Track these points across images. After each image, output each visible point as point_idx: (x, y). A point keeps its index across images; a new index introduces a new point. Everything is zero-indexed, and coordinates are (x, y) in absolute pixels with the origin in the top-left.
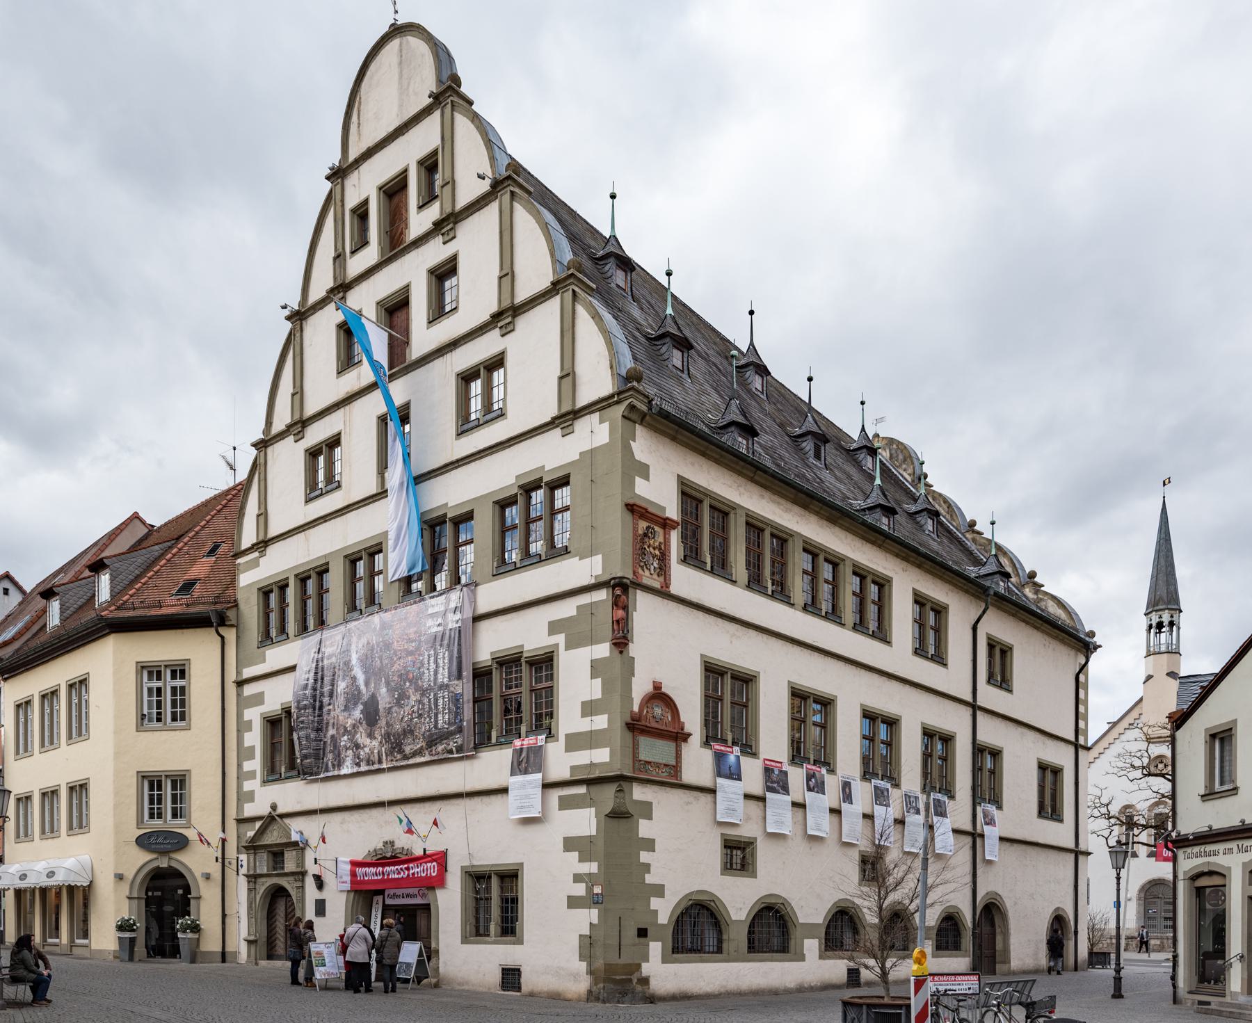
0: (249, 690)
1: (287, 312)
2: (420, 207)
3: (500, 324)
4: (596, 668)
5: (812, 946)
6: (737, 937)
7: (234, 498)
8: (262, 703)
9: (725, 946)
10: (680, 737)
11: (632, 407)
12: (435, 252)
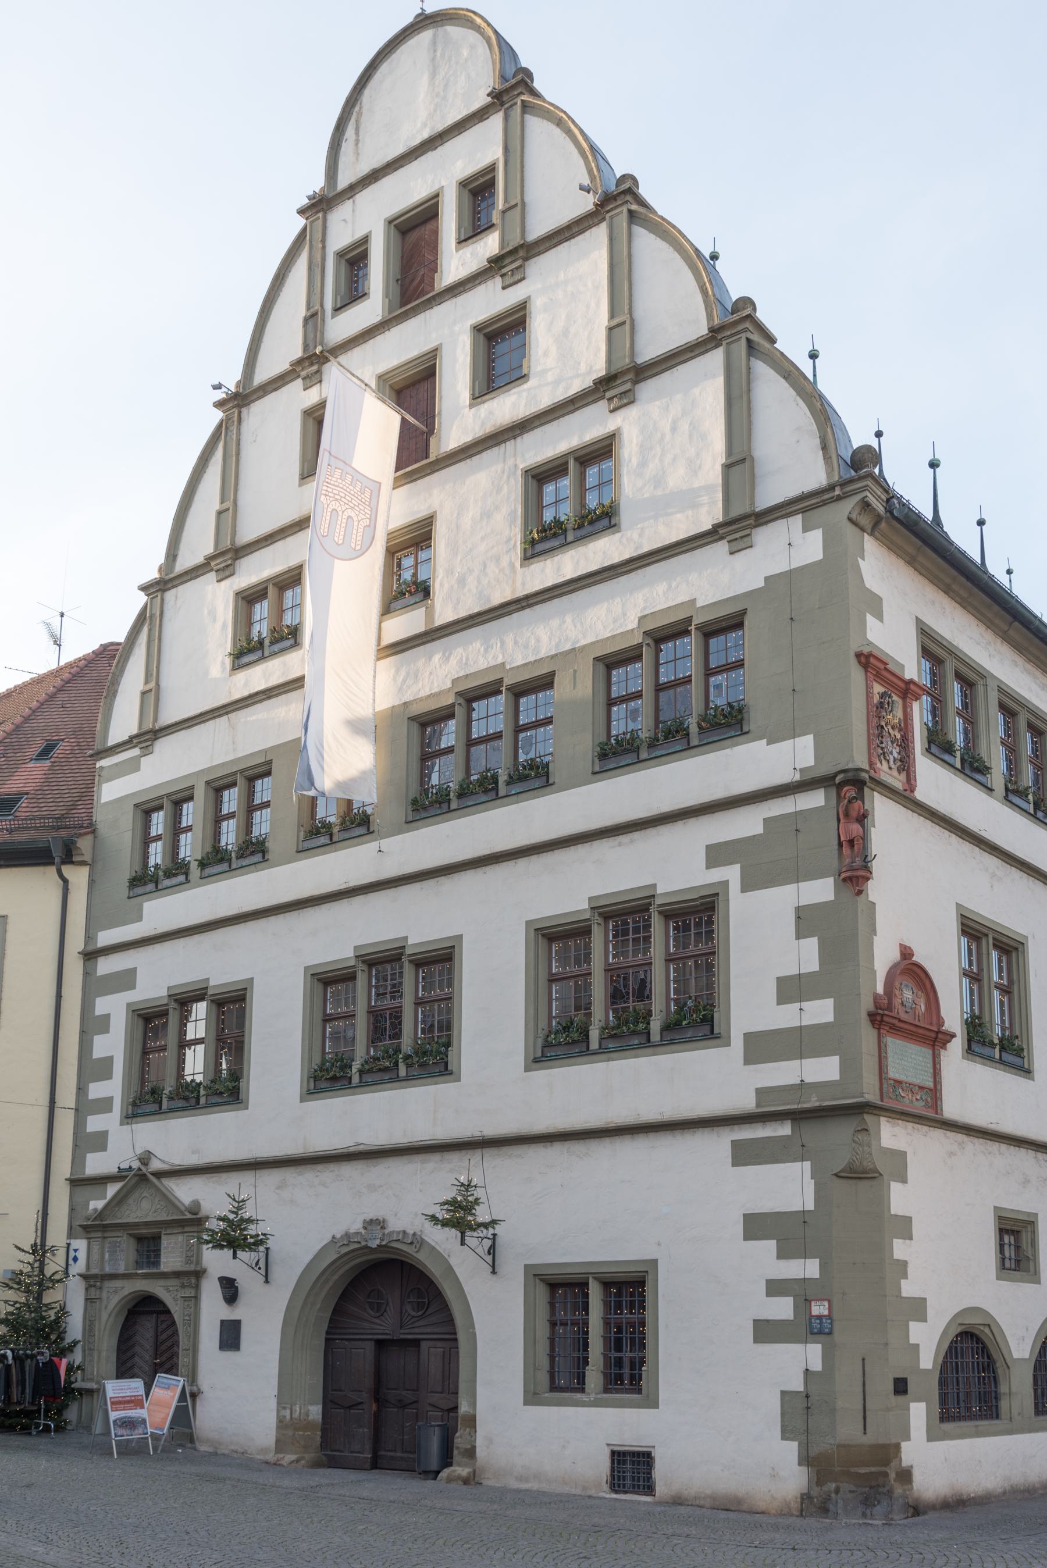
0: (106, 966)
1: (220, 395)
3: (608, 395)
4: (806, 920)
7: (101, 668)
8: (132, 986)
9: (1004, 1404)
10: (936, 1039)
11: (866, 505)
12: (490, 301)
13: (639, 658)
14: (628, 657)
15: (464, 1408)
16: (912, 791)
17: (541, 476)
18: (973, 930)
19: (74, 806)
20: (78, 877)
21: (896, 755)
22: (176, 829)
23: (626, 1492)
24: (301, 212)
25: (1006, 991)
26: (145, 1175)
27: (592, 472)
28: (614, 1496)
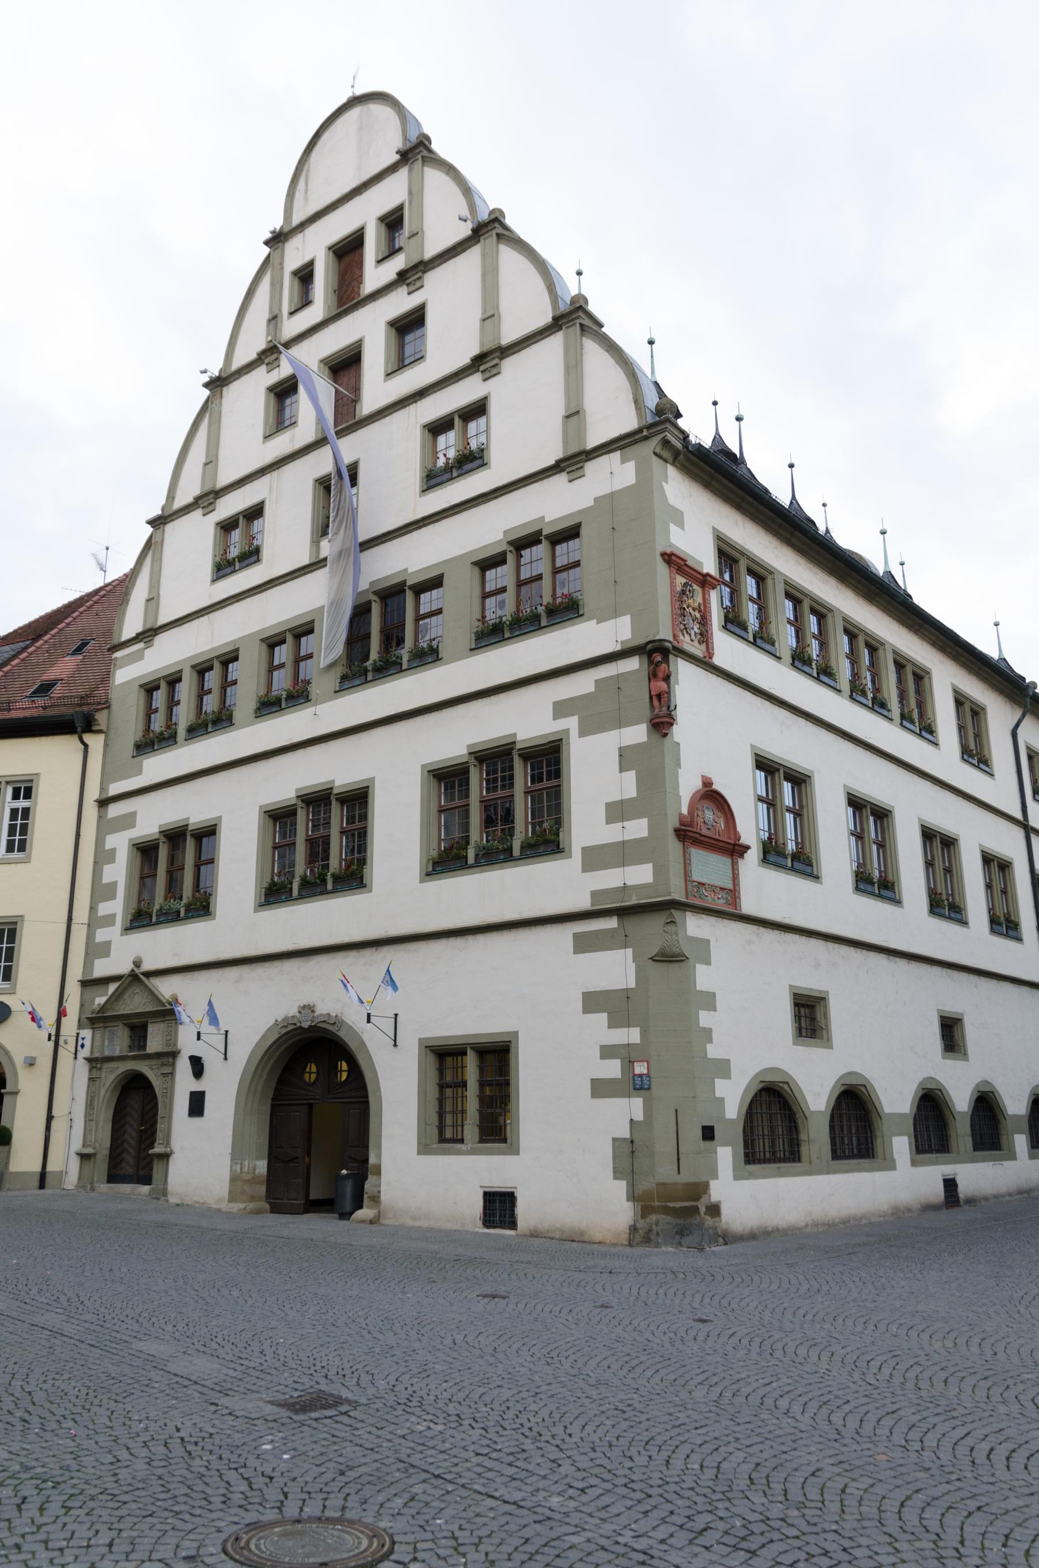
0: (115, 810)
1: (206, 378)
2: (379, 262)
3: (482, 368)
4: (626, 758)
5: (901, 1146)
6: (817, 1134)
9: (804, 1149)
10: (736, 850)
11: (666, 443)
12: (400, 303)
13: (503, 562)
14: (495, 561)
15: (372, 1160)
16: (711, 658)
17: (437, 428)
18: (765, 765)
19: (97, 688)
20: (96, 742)
21: (697, 631)
22: (172, 702)
23: (495, 1227)
24: (267, 243)
25: (798, 814)
26: (136, 975)
27: (472, 426)
28: (486, 1231)
